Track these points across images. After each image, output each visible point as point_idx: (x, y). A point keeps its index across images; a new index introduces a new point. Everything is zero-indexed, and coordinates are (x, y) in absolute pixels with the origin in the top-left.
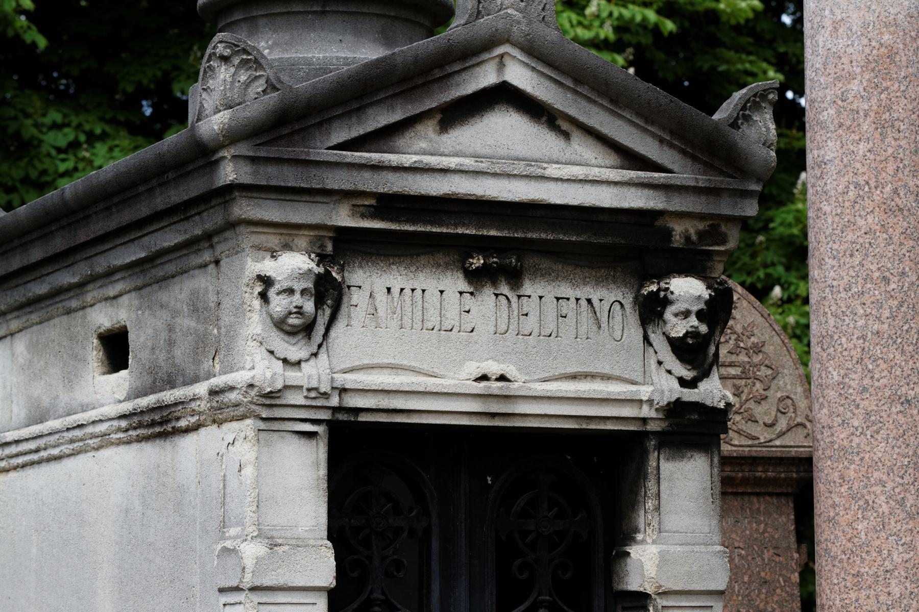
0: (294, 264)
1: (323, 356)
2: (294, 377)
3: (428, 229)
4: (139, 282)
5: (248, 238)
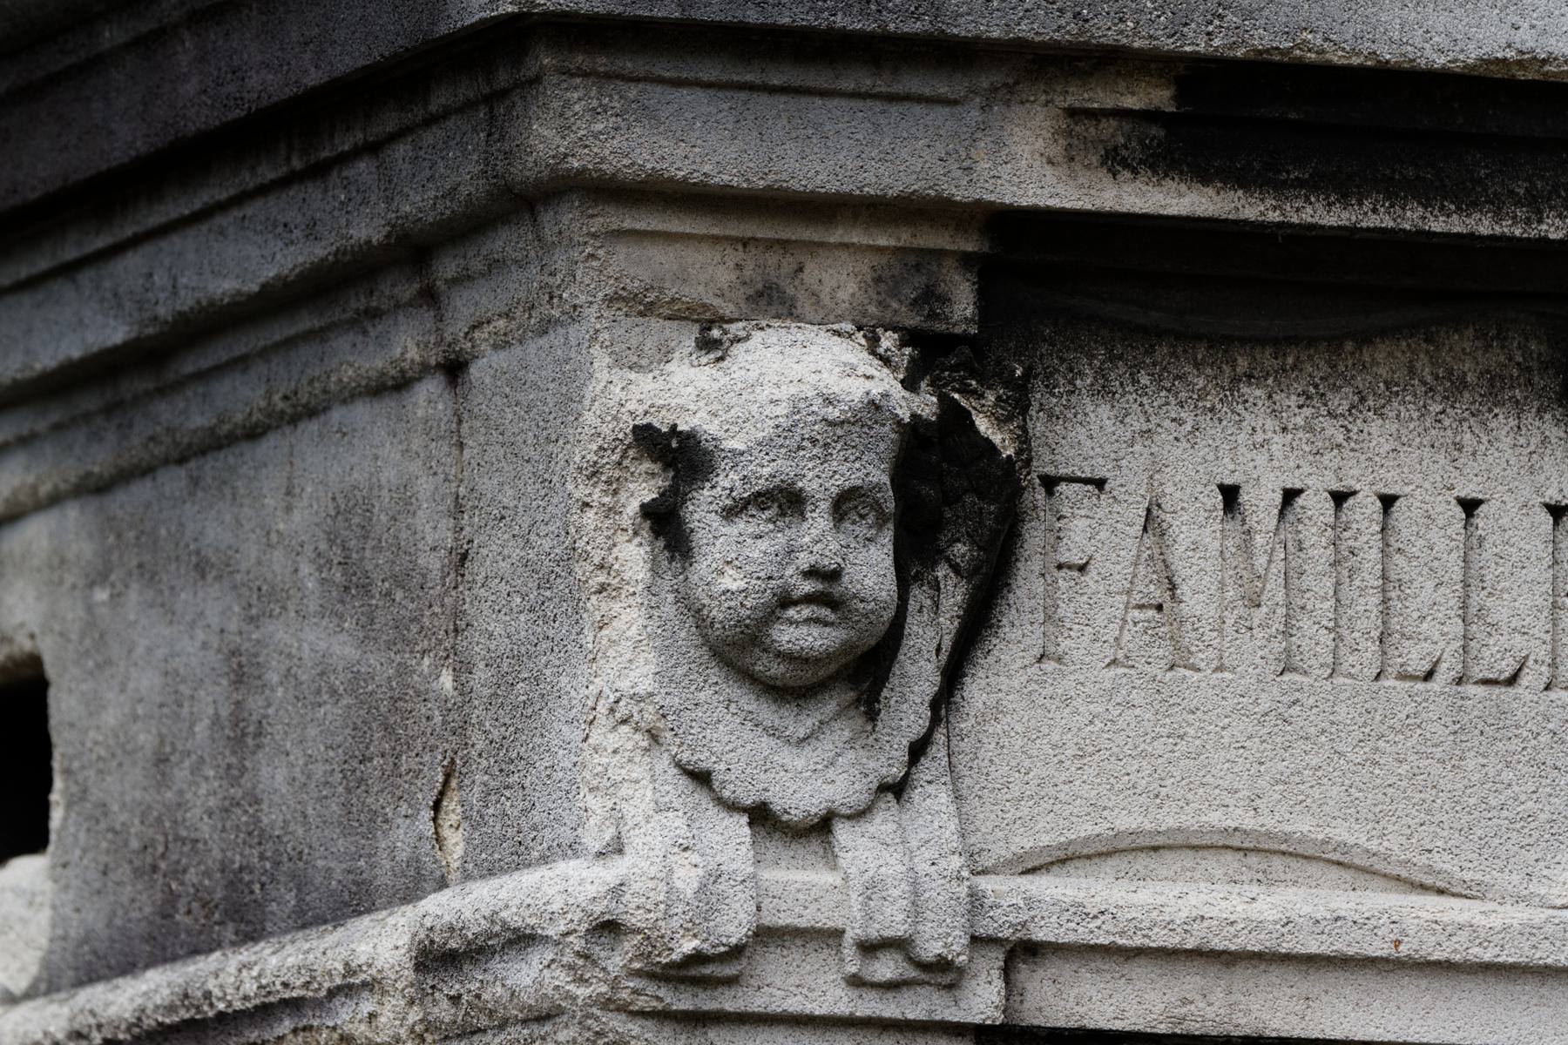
0: (799, 378)
1: (932, 799)
2: (801, 886)
3: (1412, 218)
4: (100, 459)
5: (592, 261)
